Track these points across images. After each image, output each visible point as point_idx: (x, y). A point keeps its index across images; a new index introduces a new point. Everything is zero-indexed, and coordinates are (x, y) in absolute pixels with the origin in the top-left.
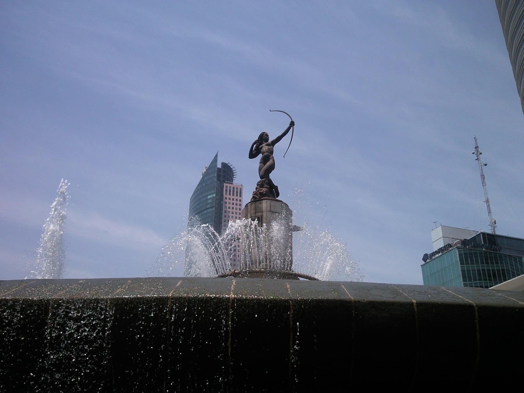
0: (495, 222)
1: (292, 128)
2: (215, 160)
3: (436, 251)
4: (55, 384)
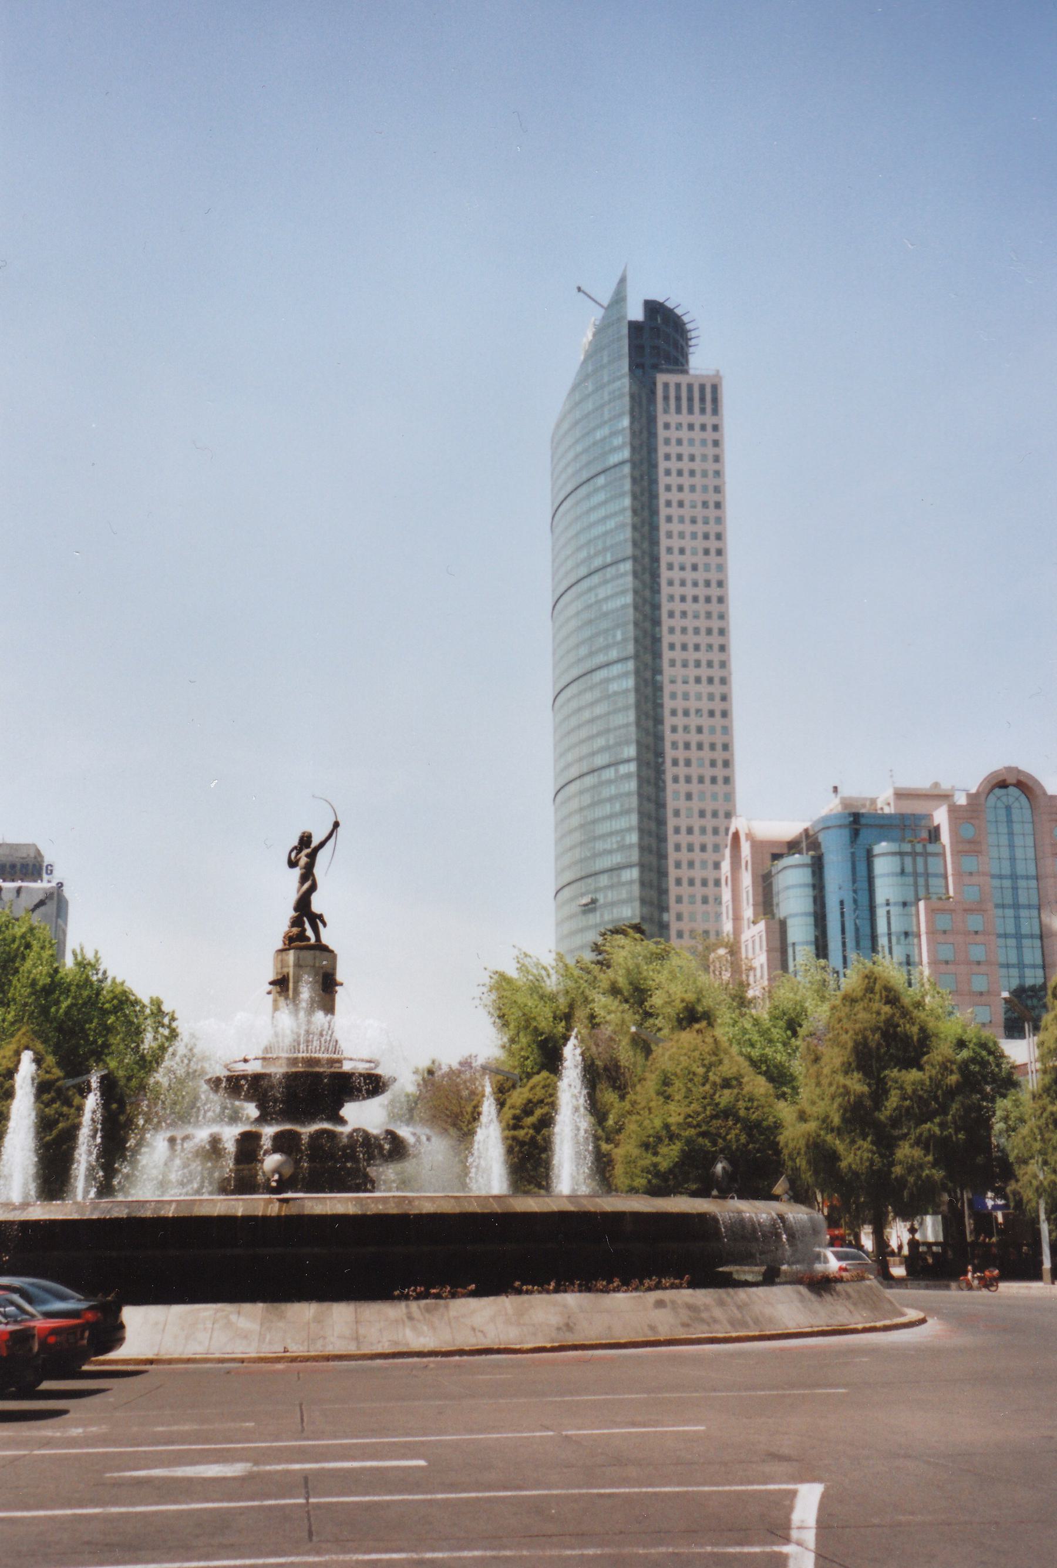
2: (619, 298)
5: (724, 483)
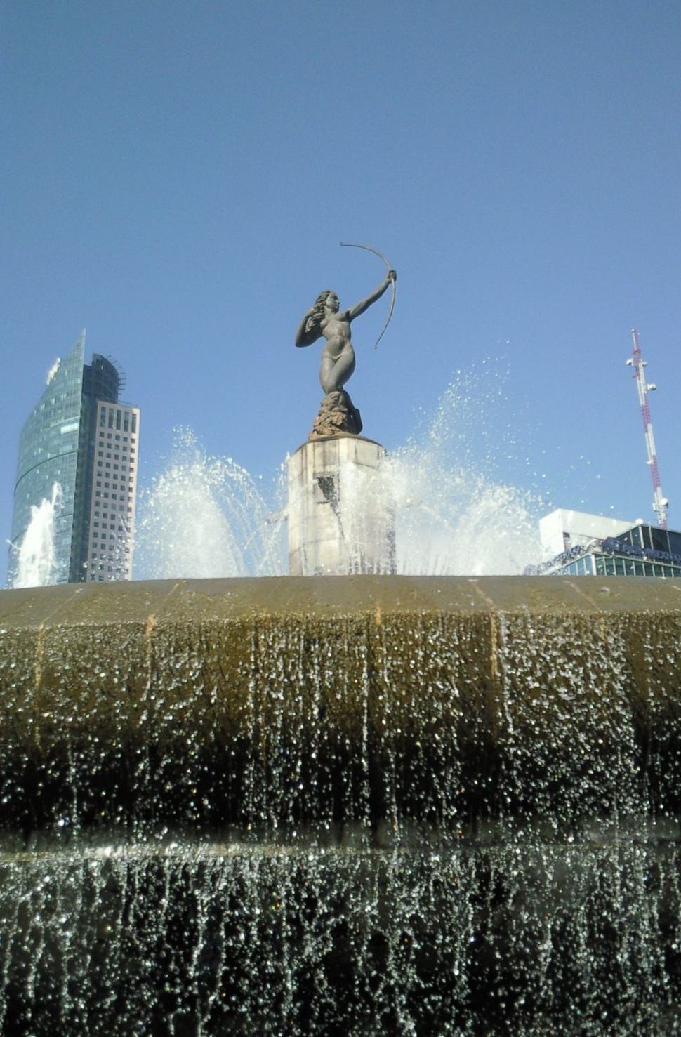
4: (496, 951)
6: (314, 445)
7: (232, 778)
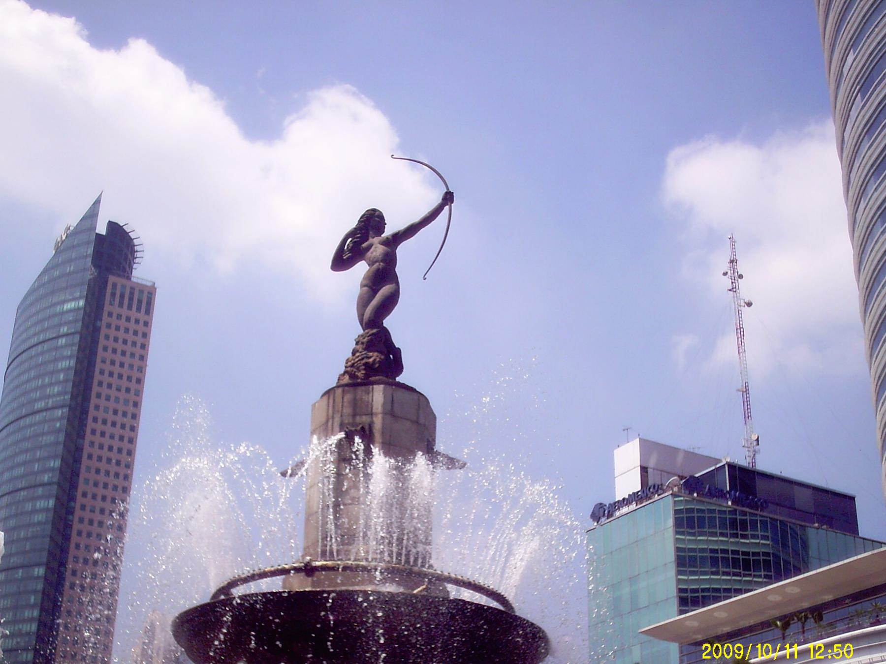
0: (757, 440)
1: (447, 208)
2: (92, 214)
3: (624, 499)
5: (146, 366)
6: (343, 391)
7: (367, 577)
